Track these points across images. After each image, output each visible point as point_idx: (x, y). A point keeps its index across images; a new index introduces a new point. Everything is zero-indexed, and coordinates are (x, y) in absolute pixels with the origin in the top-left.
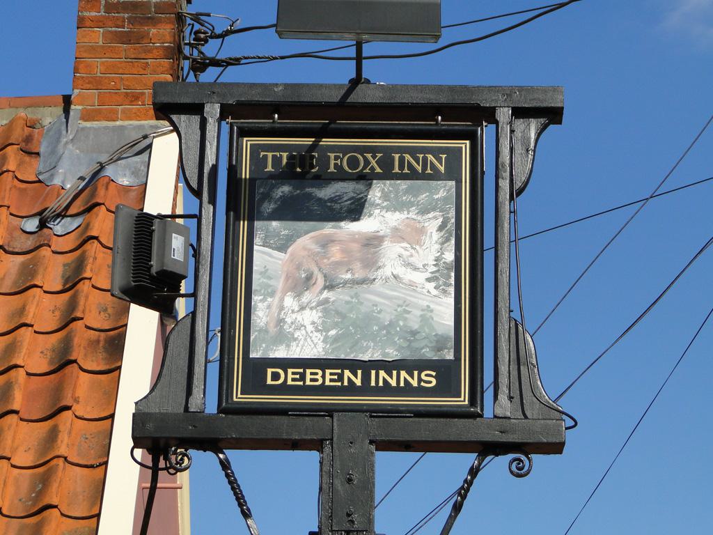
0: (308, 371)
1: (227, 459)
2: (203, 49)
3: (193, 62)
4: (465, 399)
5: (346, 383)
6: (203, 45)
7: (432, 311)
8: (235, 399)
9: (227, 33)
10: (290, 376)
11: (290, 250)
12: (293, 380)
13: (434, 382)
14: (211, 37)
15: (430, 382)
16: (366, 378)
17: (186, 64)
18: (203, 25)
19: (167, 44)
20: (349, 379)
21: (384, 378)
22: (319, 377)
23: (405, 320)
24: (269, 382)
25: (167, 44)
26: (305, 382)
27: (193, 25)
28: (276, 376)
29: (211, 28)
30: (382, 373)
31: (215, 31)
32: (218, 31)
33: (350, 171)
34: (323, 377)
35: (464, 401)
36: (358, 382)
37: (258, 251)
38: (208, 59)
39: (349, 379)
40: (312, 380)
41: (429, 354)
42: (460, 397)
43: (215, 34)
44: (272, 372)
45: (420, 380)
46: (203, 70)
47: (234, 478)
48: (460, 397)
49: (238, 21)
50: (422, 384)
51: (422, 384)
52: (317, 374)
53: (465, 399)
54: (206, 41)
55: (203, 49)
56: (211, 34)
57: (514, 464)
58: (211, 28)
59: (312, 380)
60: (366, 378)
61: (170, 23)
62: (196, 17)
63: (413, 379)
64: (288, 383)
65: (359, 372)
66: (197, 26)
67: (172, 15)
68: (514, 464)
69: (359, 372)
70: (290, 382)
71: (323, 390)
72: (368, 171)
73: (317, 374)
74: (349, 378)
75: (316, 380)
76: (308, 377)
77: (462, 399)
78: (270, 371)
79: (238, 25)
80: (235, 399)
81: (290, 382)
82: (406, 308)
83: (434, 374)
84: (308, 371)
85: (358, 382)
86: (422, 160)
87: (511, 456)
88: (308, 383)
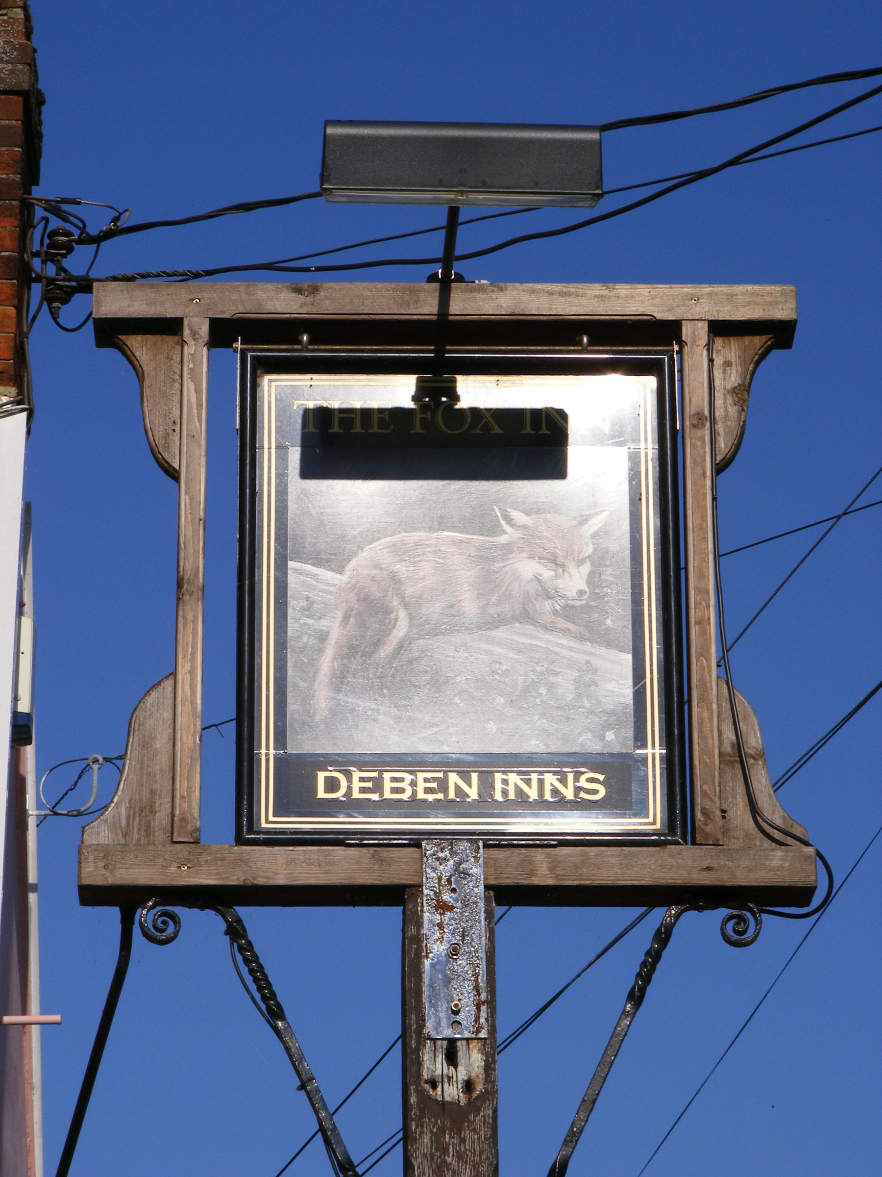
0: (387, 776)
1: (239, 921)
2: (66, 263)
3: (48, 284)
4: (655, 819)
5: (452, 795)
6: (64, 256)
7: (595, 671)
8: (264, 825)
9: (109, 235)
10: (356, 785)
11: (349, 567)
12: (363, 790)
13: (602, 792)
14: (80, 241)
15: (596, 792)
16: (487, 785)
17: (37, 289)
18: (66, 220)
19: (6, 254)
20: (457, 787)
21: (456, 784)
22: (405, 785)
23: (551, 687)
24: (321, 794)
25: (6, 254)
26: (381, 795)
27: (46, 220)
28: (332, 785)
29: (81, 225)
30: (513, 778)
31: (88, 229)
32: (93, 230)
33: (449, 432)
34: (413, 784)
35: (267, 822)
36: (473, 793)
37: (296, 571)
38: (72, 278)
39: (457, 787)
40: (395, 790)
41: (590, 744)
42: (274, 816)
43: (87, 234)
44: (326, 778)
45: (578, 790)
46: (65, 301)
47: (636, 982)
48: (274, 816)
49: (127, 214)
50: (583, 795)
51: (583, 795)
52: (402, 780)
53: (655, 819)
54: (70, 250)
55: (66, 263)
56: (80, 235)
57: (731, 924)
58: (81, 225)
59: (395, 790)
60: (487, 785)
61: (11, 216)
62: (54, 208)
63: (566, 787)
64: (319, 796)
65: (475, 777)
66: (55, 223)
67: (14, 202)
68: (731, 924)
69: (475, 777)
70: (356, 795)
71: (415, 806)
72: (478, 431)
73: (402, 780)
74: (470, 785)
75: (402, 791)
76: (388, 785)
77: (271, 818)
78: (321, 776)
79: (125, 221)
80: (264, 825)
81: (356, 795)
82: (552, 667)
83: (601, 777)
84: (387, 776)
85: (473, 793)
86: (531, 420)
87: (723, 912)
88: (388, 795)
